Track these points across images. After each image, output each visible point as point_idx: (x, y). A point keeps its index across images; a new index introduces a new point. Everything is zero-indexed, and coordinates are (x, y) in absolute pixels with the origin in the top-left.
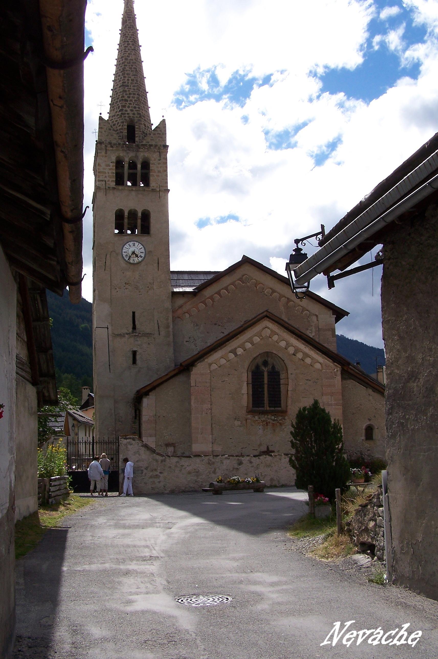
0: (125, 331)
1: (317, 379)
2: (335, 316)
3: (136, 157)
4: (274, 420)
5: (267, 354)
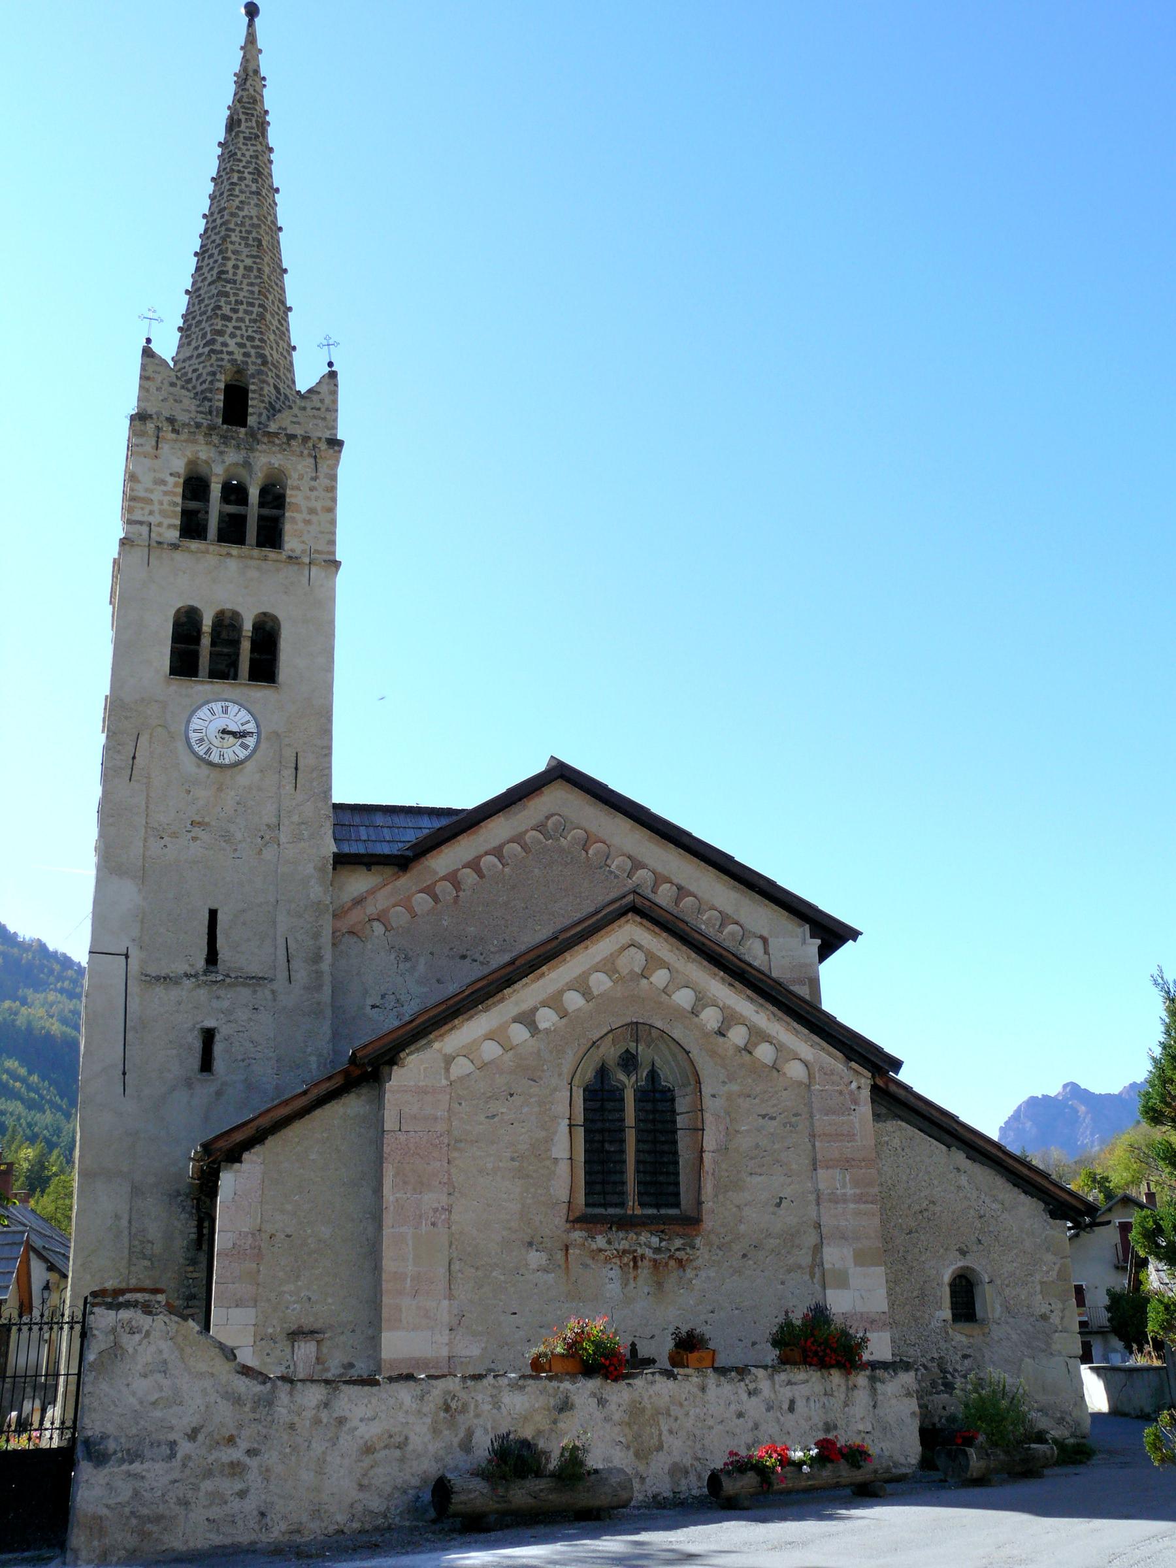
0: (181, 967)
3: (247, 464)
4: (657, 1250)
5: (635, 1029)
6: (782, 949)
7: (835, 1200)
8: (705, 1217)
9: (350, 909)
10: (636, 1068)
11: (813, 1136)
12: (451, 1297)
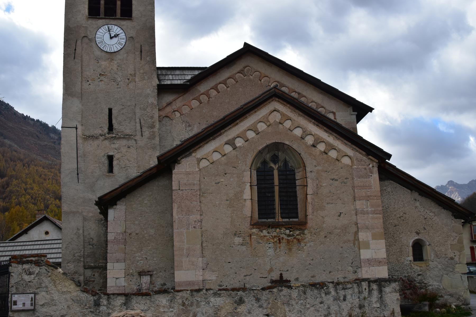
1: (346, 179)
2: (356, 113)
4: (289, 236)
6: (342, 117)
7: (363, 213)
8: (309, 222)
9: (166, 107)
10: (278, 162)
11: (353, 187)
12: (203, 257)
